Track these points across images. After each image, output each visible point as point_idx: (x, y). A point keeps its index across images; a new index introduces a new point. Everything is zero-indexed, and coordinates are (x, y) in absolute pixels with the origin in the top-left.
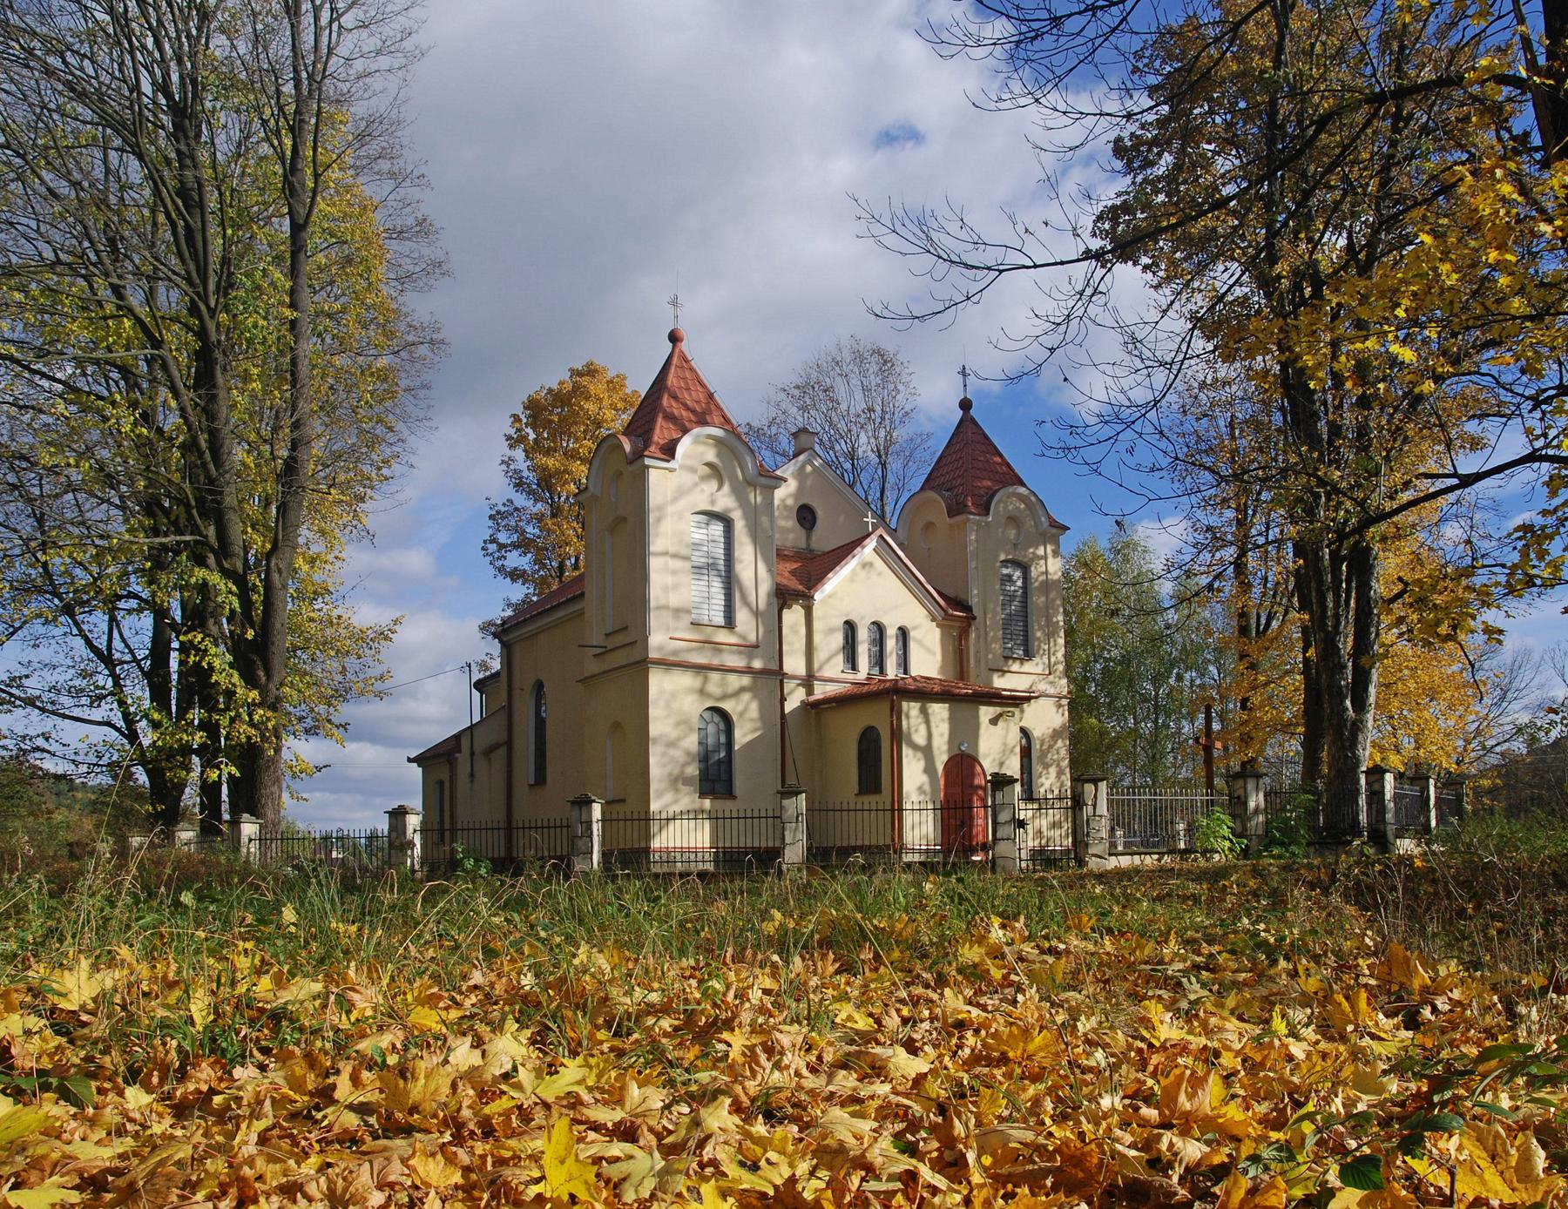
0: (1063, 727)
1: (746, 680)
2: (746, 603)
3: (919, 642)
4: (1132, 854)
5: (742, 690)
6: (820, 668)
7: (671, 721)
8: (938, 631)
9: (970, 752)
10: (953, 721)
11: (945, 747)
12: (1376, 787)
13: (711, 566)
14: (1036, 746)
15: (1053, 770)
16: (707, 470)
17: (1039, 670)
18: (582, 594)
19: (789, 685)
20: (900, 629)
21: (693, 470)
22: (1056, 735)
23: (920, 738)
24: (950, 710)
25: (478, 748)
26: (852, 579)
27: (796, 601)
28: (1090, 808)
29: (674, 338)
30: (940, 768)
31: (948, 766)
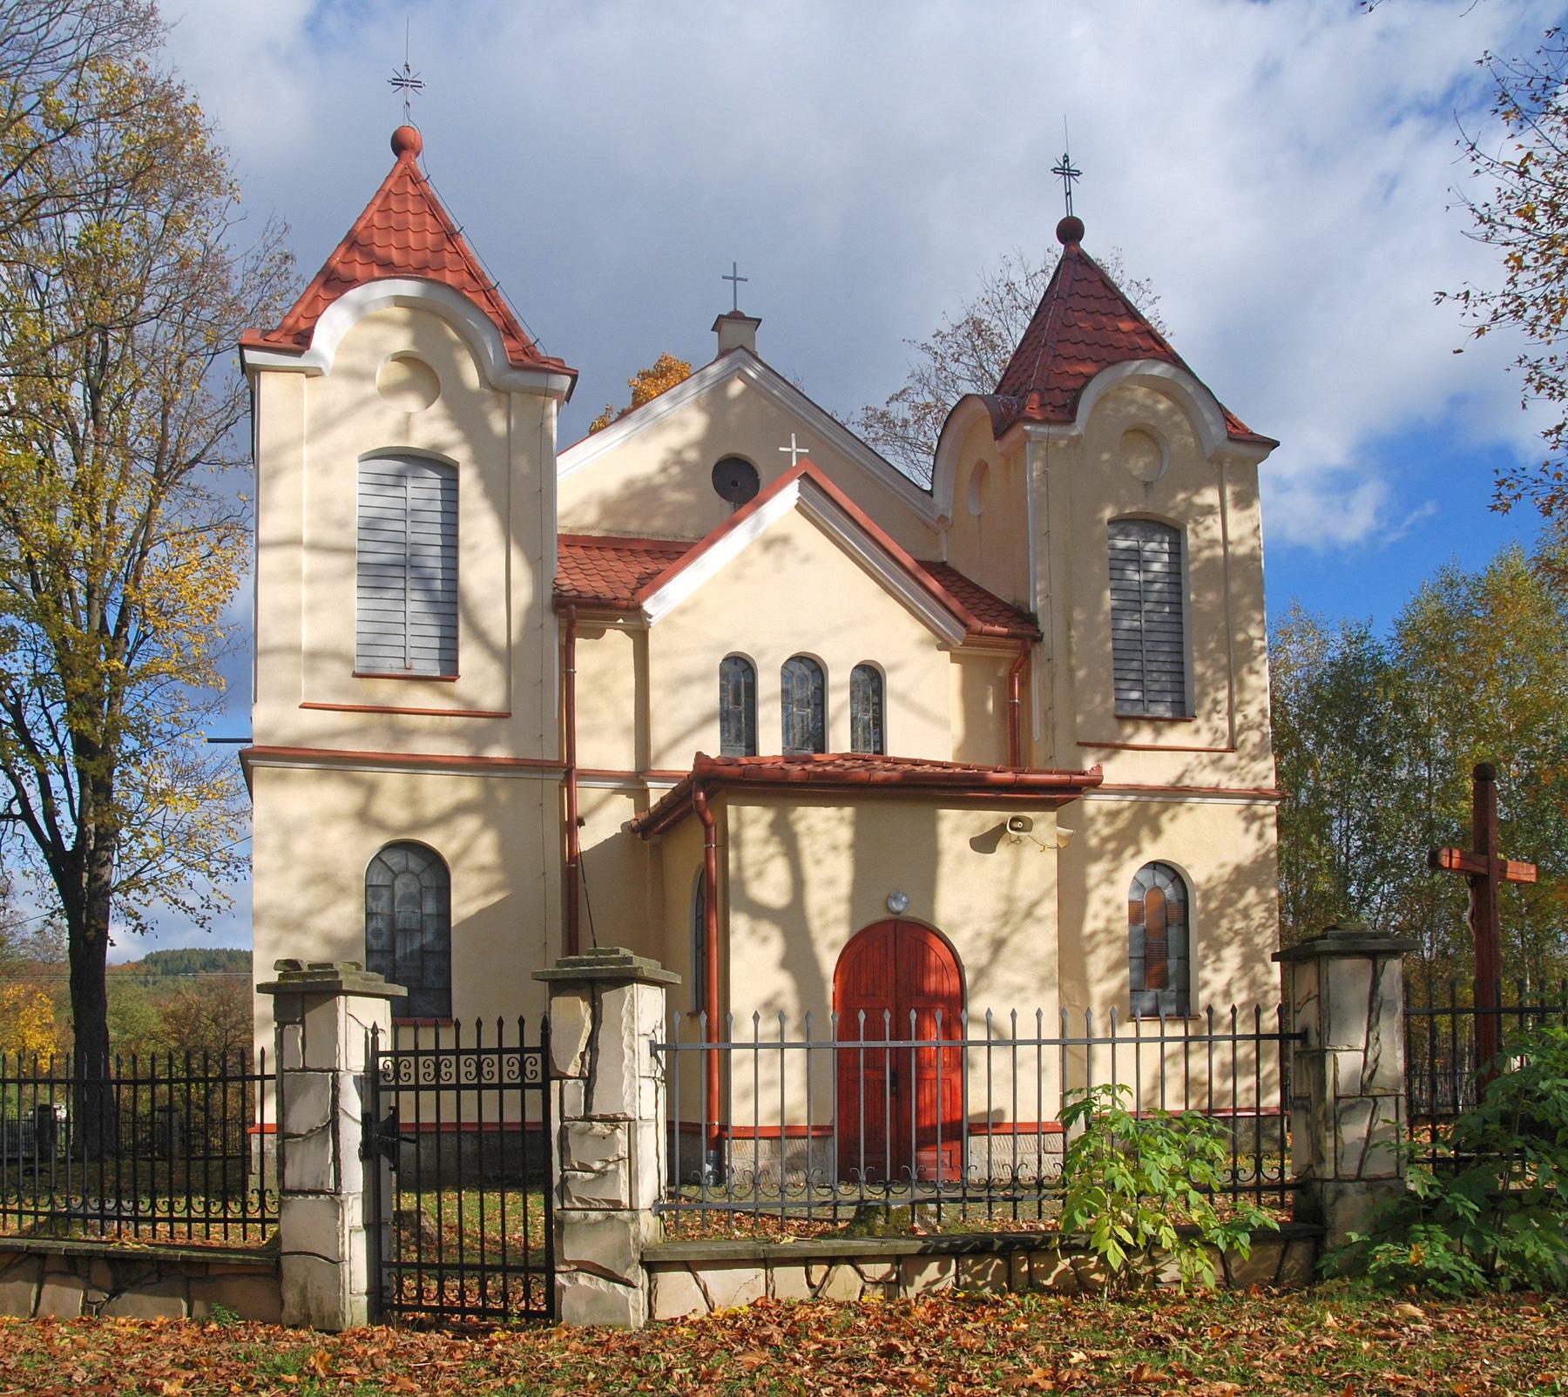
0: (1260, 863)
1: (468, 789)
2: (481, 636)
3: (902, 698)
4: (767, 1261)
5: (462, 809)
6: (659, 757)
7: (296, 875)
8: (955, 670)
9: (915, 913)
10: (863, 851)
11: (841, 910)
13: (408, 565)
14: (1196, 903)
15: (1232, 956)
16: (399, 372)
17: (1204, 740)
19: (587, 795)
20: (801, 659)
21: (357, 375)
22: (1242, 877)
23: (770, 887)
24: (858, 825)
26: (737, 574)
27: (611, 621)
28: (574, 1091)
29: (400, 145)
30: (829, 962)
31: (851, 956)
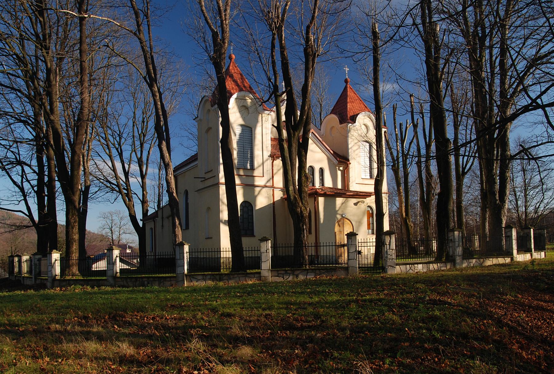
12: (509, 234)
18: (197, 158)
25: (164, 216)
28: (388, 246)
